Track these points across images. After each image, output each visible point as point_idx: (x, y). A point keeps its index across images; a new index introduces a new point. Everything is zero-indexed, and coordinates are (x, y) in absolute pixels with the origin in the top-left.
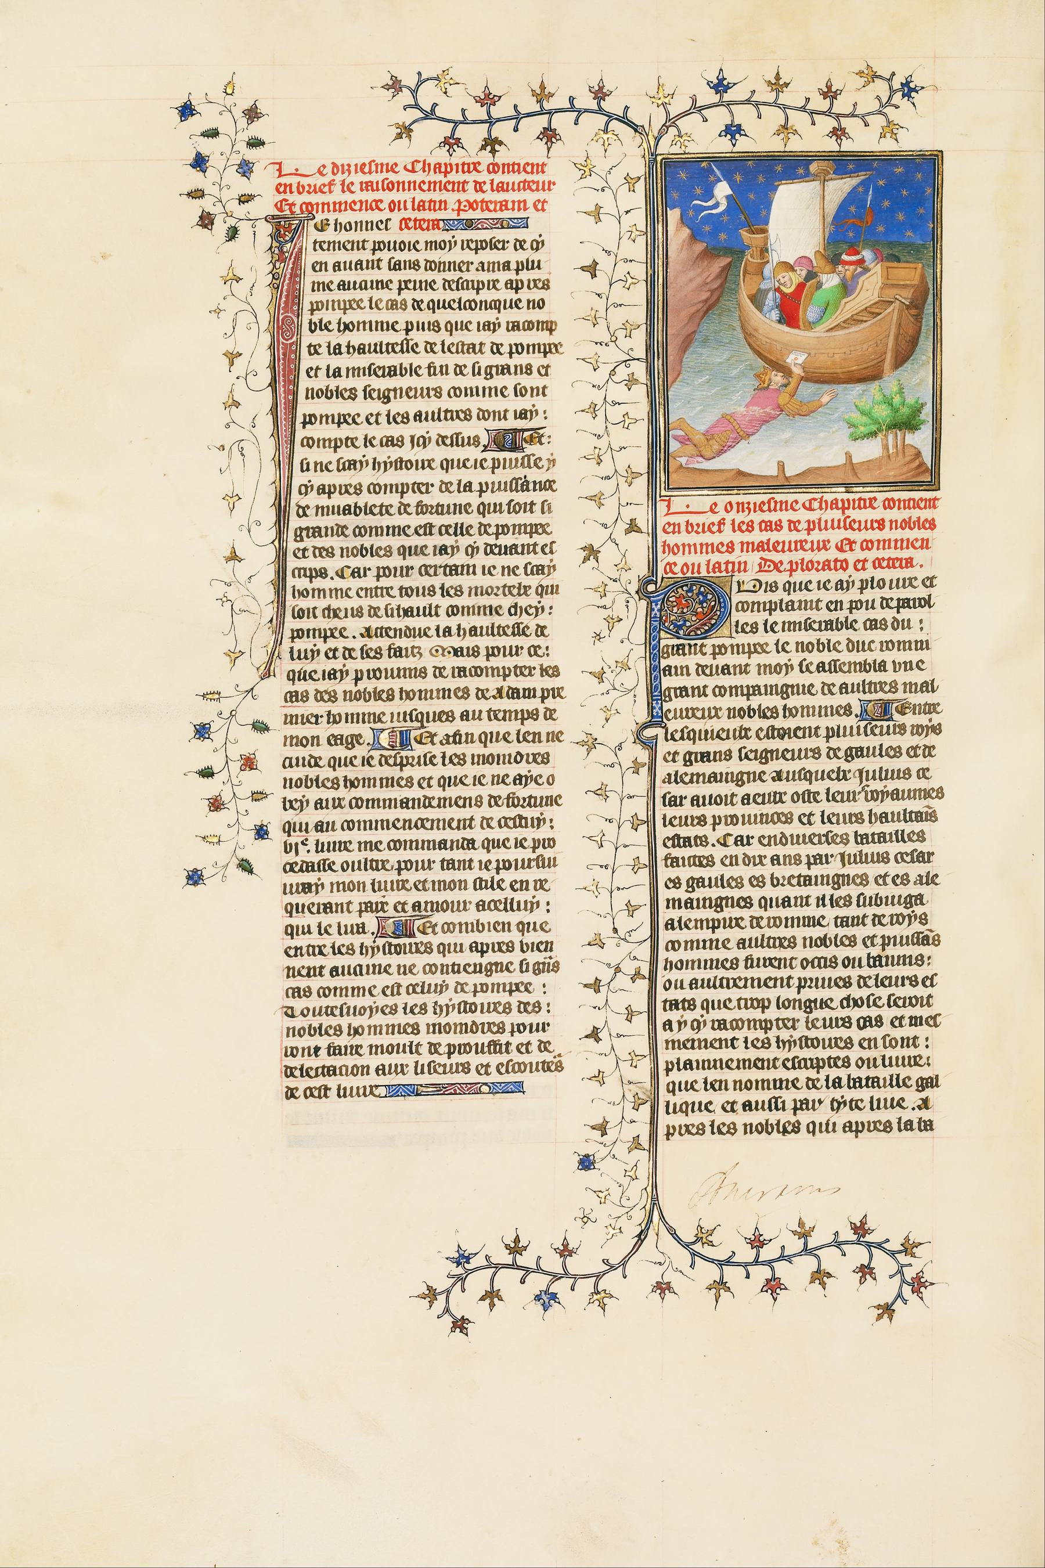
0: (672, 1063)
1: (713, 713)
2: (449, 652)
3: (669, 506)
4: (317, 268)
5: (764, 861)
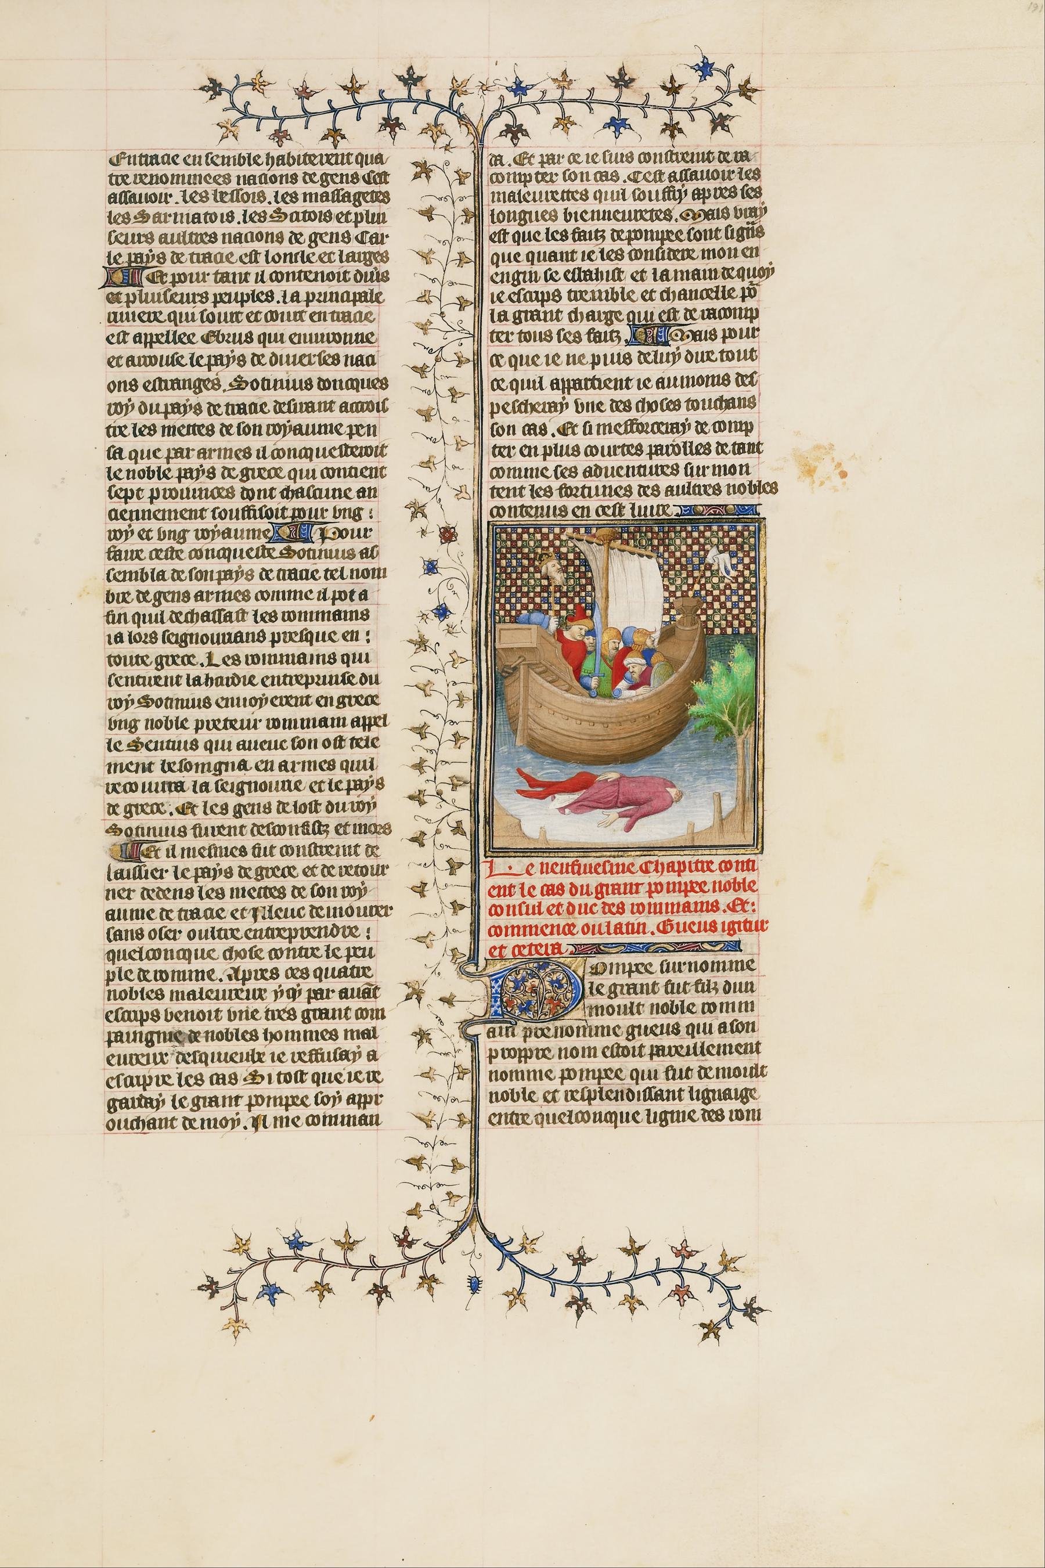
3: (491, 868)
4: (349, 638)
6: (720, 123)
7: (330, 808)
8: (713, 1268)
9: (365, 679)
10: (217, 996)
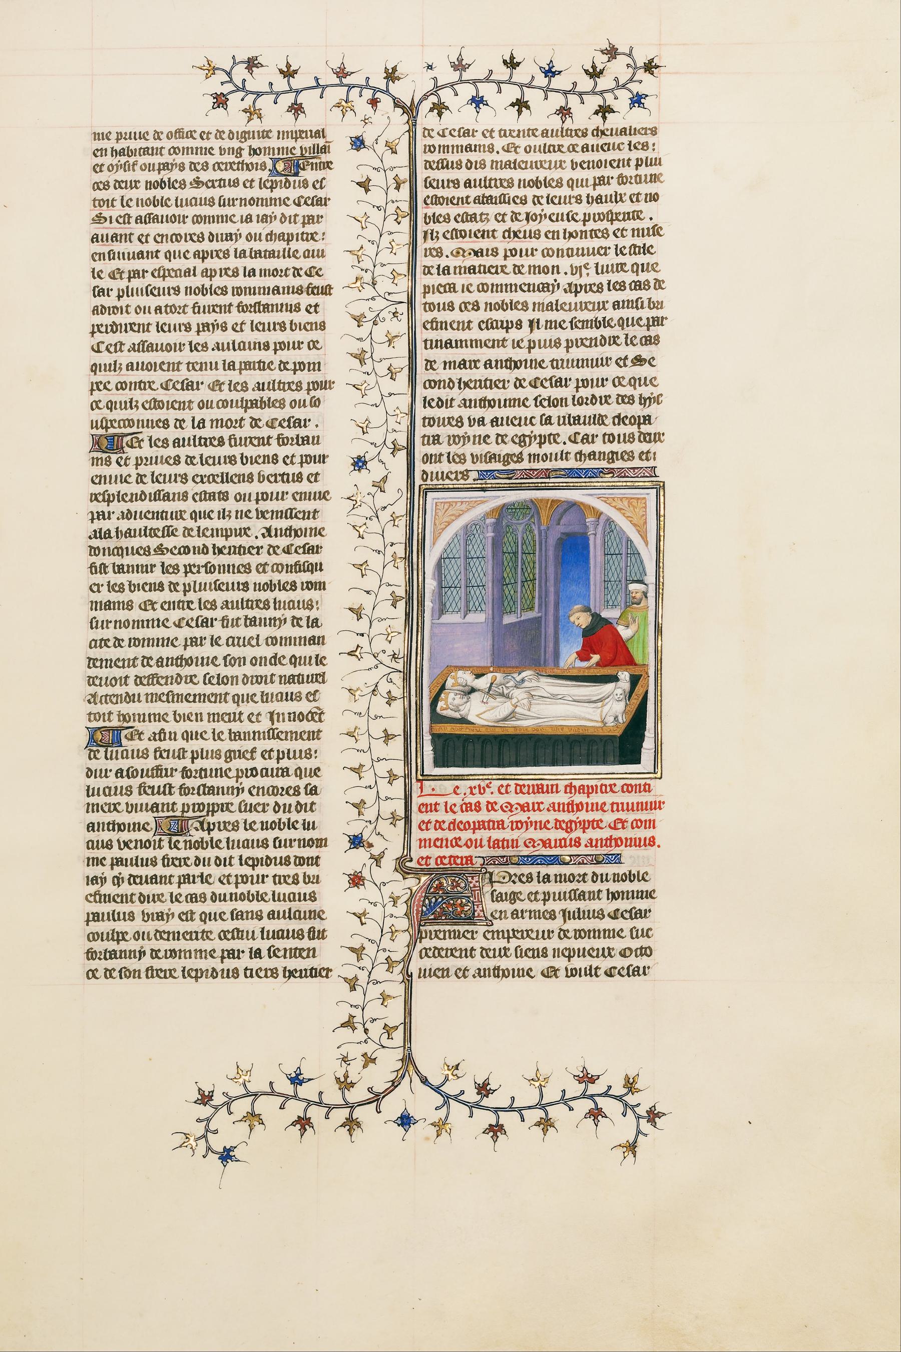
0: (641, 159)
1: (536, 807)
2: (516, 809)
3: (421, 788)
5: (607, 306)
6: (637, 100)
7: (277, 809)
8: (618, 1090)
9: (308, 880)
10: (598, 954)
